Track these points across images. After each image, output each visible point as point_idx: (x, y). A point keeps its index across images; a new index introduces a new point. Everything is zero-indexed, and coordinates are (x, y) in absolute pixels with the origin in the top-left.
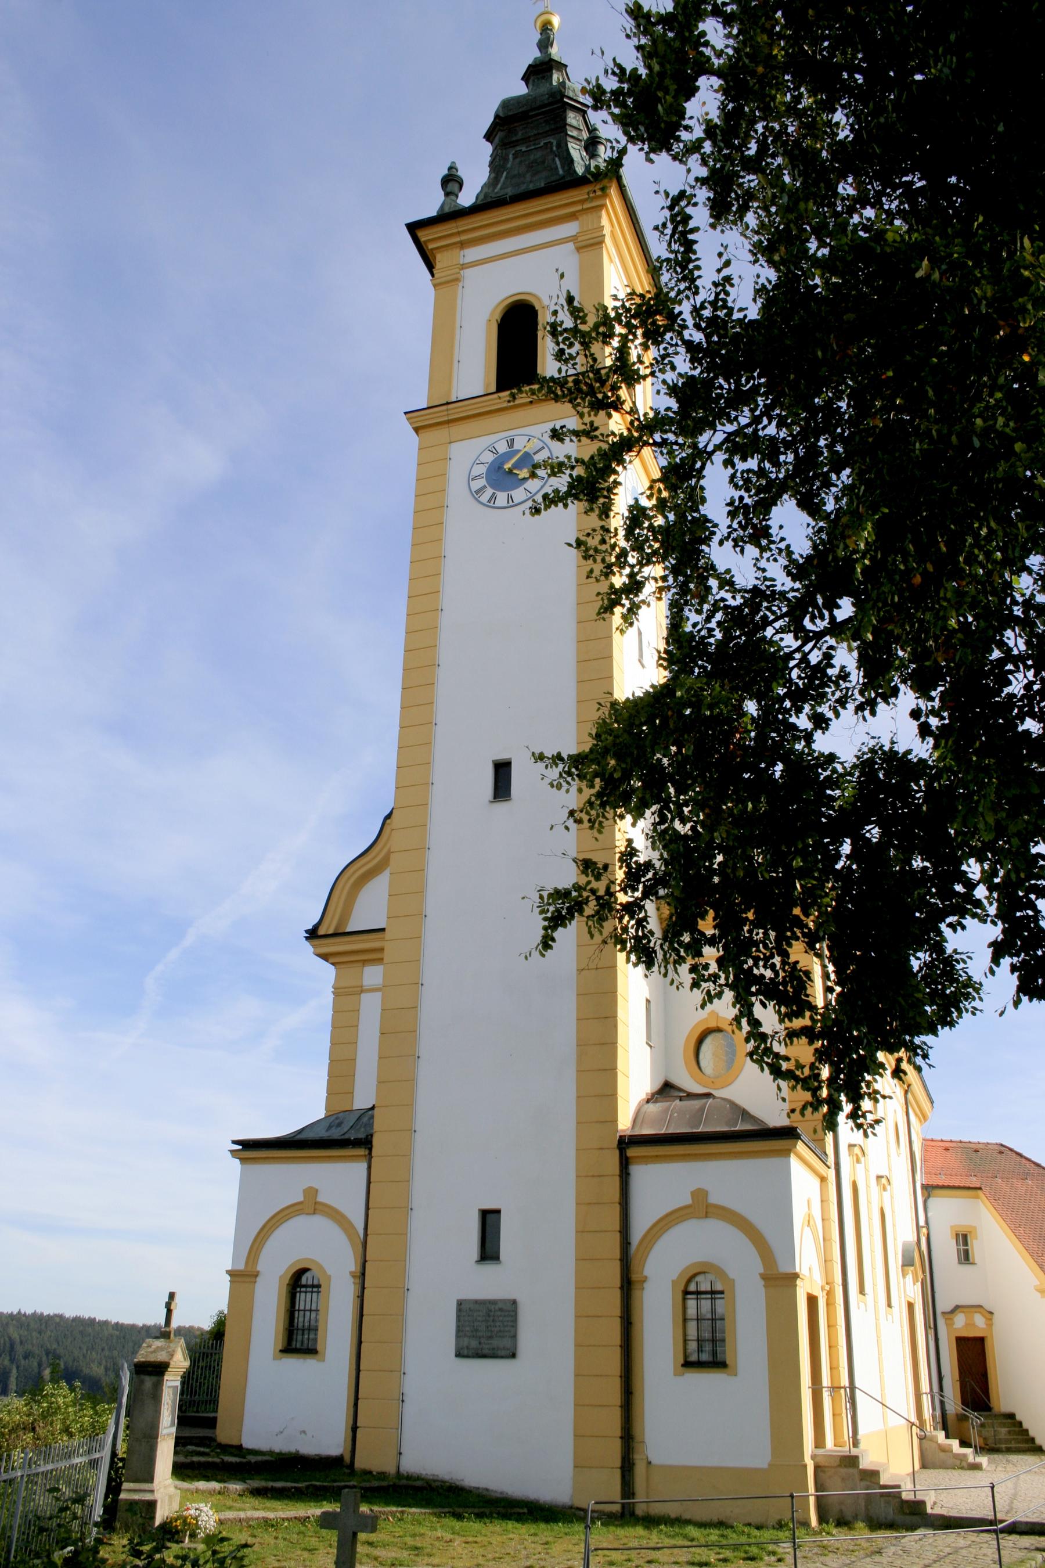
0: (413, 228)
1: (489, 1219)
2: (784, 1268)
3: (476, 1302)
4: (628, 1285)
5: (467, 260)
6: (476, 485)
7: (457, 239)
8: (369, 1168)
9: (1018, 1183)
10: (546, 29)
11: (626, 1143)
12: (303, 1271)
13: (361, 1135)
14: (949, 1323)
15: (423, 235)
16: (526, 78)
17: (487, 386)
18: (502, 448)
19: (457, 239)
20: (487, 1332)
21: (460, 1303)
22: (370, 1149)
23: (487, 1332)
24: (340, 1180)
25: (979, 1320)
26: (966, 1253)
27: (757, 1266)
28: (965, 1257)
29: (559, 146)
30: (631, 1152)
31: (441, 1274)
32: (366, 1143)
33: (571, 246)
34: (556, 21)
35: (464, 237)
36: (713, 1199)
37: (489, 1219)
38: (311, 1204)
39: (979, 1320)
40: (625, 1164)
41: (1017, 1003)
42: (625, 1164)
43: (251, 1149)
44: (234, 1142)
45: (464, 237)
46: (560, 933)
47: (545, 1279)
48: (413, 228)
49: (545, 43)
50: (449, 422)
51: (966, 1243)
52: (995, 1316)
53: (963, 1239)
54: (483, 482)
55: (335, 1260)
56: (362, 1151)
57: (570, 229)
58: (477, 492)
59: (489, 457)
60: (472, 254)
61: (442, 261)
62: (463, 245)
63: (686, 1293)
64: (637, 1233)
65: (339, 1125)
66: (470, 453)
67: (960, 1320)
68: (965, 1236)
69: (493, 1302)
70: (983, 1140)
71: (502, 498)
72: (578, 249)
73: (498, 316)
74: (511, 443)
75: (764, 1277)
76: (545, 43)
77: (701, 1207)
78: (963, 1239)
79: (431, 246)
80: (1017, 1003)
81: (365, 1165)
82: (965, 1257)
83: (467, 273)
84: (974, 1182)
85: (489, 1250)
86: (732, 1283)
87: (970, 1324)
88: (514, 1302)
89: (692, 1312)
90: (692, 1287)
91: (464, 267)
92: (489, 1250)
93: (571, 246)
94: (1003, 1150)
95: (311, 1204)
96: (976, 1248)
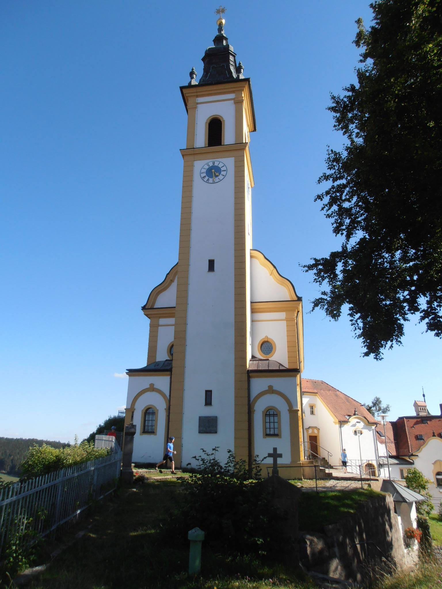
0: (182, 88)
1: (208, 394)
2: (295, 409)
3: (205, 417)
4: (250, 412)
5: (199, 102)
6: (203, 175)
7: (195, 94)
8: (171, 378)
9: (327, 392)
10: (220, 25)
11: (249, 372)
12: (149, 408)
13: (169, 368)
14: (307, 431)
15: (185, 91)
16: (214, 41)
17: (205, 144)
18: (211, 164)
19: (195, 94)
20: (208, 425)
21: (200, 418)
22: (172, 373)
23: (208, 425)
24: (162, 382)
25: (316, 431)
26: (313, 411)
27: (287, 407)
28: (312, 413)
29: (227, 66)
30: (251, 374)
31: (193, 409)
32: (170, 370)
33: (233, 101)
34: (224, 21)
35: (198, 94)
36: (275, 388)
37: (208, 394)
38: (152, 388)
39: (316, 431)
40: (249, 378)
41: (427, 331)
42: (249, 378)
43: (131, 372)
44: (127, 370)
45: (198, 94)
46: (316, 308)
47: (225, 410)
48: (182, 88)
49: (220, 29)
50: (194, 154)
51: (312, 409)
52: (320, 431)
53: (312, 407)
54: (205, 175)
55: (160, 404)
56: (169, 373)
57: (232, 96)
58: (203, 177)
59: (207, 167)
60: (200, 100)
61: (190, 102)
62: (197, 96)
63: (266, 415)
64: (252, 399)
65: (158, 365)
66: (200, 166)
67: (310, 431)
68: (312, 407)
69: (210, 417)
70: (317, 379)
71: (211, 180)
72: (235, 103)
73: (209, 122)
74: (214, 163)
75: (289, 410)
76: (220, 29)
77: (271, 390)
78: (312, 407)
79: (187, 95)
80: (427, 331)
81: (169, 377)
82: (312, 413)
83: (199, 106)
84: (315, 391)
85: (208, 402)
86: (280, 412)
87: (313, 432)
88: (216, 417)
89: (268, 420)
90: (268, 413)
91: (198, 104)
92: (208, 402)
93: (233, 101)
94: (323, 382)
95: (152, 388)
96: (315, 410)
